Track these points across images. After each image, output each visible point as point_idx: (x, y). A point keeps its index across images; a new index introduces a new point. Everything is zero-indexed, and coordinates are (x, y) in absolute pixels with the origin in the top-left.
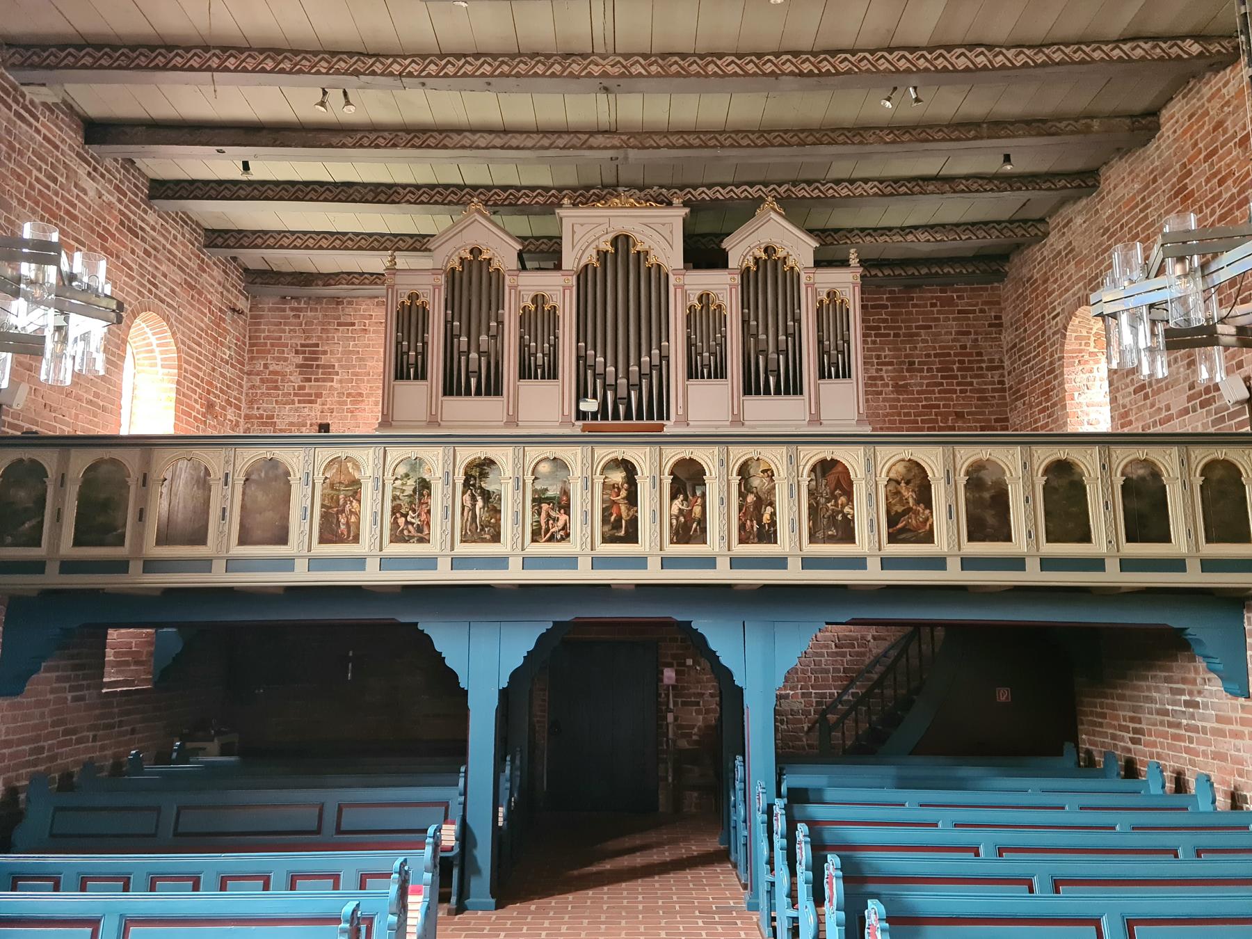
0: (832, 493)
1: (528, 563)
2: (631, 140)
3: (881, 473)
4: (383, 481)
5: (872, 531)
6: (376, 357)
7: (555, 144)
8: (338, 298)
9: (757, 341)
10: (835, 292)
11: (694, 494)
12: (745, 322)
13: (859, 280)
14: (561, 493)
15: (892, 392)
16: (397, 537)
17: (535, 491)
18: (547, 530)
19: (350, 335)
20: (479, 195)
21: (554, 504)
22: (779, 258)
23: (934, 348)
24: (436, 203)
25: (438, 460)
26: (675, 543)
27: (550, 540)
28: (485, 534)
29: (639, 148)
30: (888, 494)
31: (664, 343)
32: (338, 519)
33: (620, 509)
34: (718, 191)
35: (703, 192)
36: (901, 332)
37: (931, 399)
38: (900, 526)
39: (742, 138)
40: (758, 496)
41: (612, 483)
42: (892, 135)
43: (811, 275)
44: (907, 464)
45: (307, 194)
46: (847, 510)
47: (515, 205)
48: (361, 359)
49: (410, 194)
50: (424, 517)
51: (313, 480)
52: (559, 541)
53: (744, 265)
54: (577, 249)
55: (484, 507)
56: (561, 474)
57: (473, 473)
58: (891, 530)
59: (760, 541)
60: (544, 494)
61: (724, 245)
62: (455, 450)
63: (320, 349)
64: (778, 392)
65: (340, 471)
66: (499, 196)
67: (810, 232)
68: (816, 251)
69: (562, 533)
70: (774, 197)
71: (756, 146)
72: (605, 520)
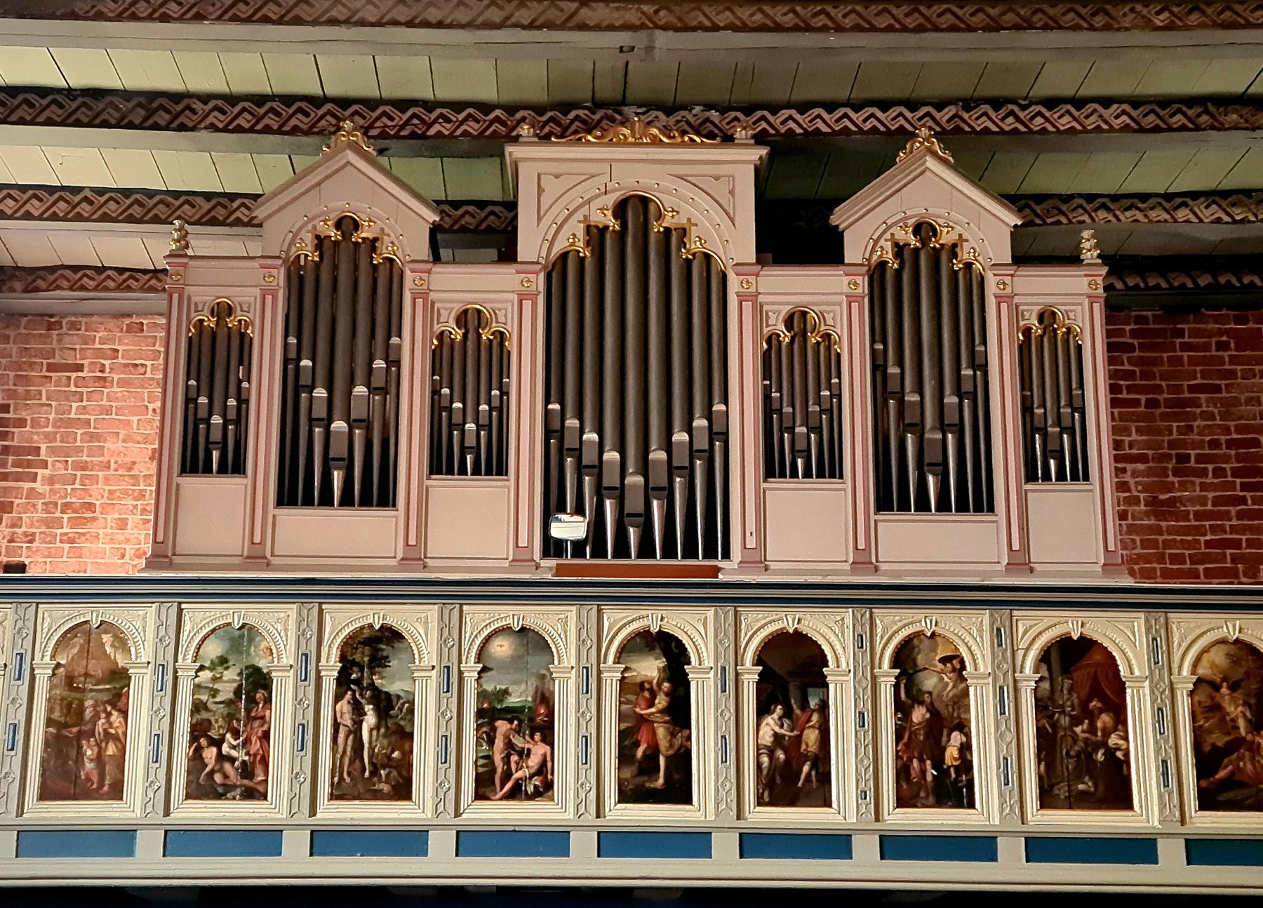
0: (1084, 705)
1: (469, 841)
2: (662, 13)
3: (1180, 667)
4: (175, 671)
5: (1166, 785)
6: (123, 433)
7: (513, 20)
8: (52, 316)
9: (901, 402)
10: (1054, 314)
11: (804, 705)
12: (878, 368)
13: (1101, 291)
14: (534, 699)
15: (1147, 514)
16: (201, 788)
17: (482, 695)
18: (507, 775)
19: (73, 388)
20: (353, 114)
21: (521, 722)
22: (942, 245)
23: (1227, 430)
24: (267, 130)
25: (286, 630)
26: (771, 804)
27: (512, 795)
28: (380, 781)
29: (677, 30)
30: (1198, 709)
31: (719, 407)
32: (80, 747)
33: (654, 734)
34: (819, 116)
35: (790, 118)
36: (1161, 398)
37: (1213, 529)
38: (1222, 774)
39: (877, 15)
40: (932, 710)
41: (638, 680)
42: (1166, 14)
43: (1008, 280)
44: (1233, 649)
45: (13, 111)
46: (1113, 740)
47: (423, 137)
48: (93, 437)
49: (216, 113)
50: (255, 746)
51: (33, 670)
52: (530, 797)
53: (875, 257)
54: (546, 221)
55: (378, 727)
56: (535, 660)
57: (358, 657)
58: (1204, 784)
59: (939, 804)
60: (501, 701)
61: (834, 220)
62: (321, 611)
63: (11, 415)
64: (943, 506)
65: (86, 651)
66: (392, 119)
67: (1013, 200)
68: (1016, 233)
69: (537, 781)
70: (930, 128)
71: (905, 29)
72: (625, 757)
